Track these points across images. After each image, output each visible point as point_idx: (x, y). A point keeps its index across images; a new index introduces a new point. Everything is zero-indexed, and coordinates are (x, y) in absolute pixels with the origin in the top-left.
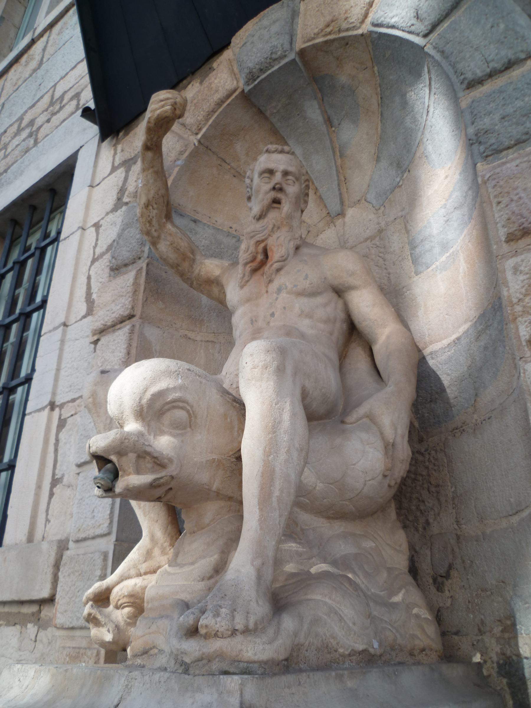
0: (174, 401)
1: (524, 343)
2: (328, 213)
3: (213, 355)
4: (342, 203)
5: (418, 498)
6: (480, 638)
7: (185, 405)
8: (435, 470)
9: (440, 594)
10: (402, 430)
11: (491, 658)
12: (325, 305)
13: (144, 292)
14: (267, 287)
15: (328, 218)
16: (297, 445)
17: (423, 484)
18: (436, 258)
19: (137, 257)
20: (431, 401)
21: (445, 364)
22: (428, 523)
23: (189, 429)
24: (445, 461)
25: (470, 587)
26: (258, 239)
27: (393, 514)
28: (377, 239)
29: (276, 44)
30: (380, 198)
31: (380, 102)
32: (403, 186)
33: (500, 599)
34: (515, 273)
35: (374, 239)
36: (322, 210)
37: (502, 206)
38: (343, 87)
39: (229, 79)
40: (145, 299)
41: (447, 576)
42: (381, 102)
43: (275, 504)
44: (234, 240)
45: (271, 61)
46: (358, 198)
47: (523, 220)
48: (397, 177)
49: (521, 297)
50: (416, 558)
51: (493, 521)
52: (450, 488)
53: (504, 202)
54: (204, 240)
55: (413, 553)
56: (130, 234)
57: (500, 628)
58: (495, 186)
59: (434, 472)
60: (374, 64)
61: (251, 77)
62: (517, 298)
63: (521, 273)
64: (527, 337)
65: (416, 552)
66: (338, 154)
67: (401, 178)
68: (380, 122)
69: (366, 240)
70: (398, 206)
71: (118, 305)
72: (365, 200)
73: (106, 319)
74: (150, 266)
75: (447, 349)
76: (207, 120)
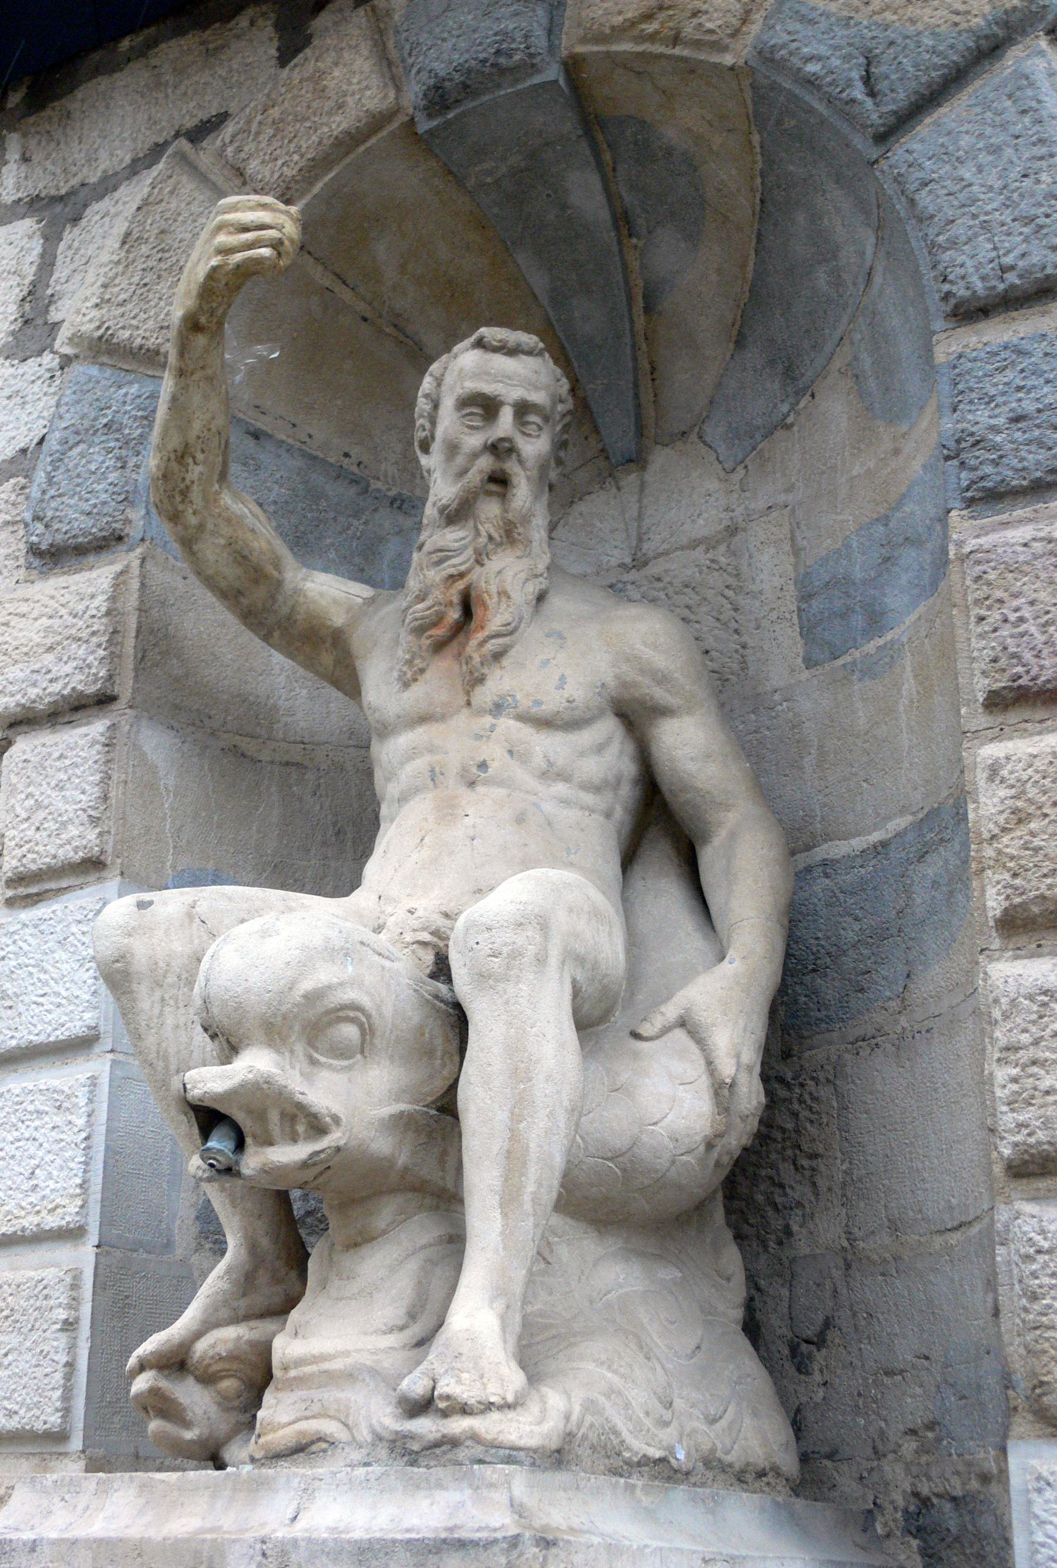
0: (344, 1007)
1: (992, 923)
2: (602, 450)
3: (301, 799)
4: (640, 431)
5: (771, 1178)
6: (876, 1463)
7: (359, 1014)
8: (812, 1122)
9: (802, 1377)
10: (751, 1056)
11: (892, 1502)
12: (600, 749)
13: (137, 637)
14: (468, 693)
15: (602, 463)
16: (566, 1103)
17: (784, 1148)
18: (855, 640)
19: (112, 534)
20: (814, 971)
21: (851, 893)
22: (788, 1232)
23: (359, 1056)
24: (835, 1104)
25: (863, 1365)
26: (453, 571)
27: (719, 1214)
28: (722, 548)
29: (511, 27)
30: (737, 442)
31: (758, 208)
32: (795, 428)
33: (918, 1390)
34: (991, 779)
35: (714, 548)
36: (586, 438)
37: (987, 629)
38: (669, 152)
39: (375, 81)
40: (140, 656)
41: (820, 1341)
42: (762, 211)
43: (528, 1206)
44: (353, 490)
45: (494, 70)
46: (684, 428)
47: (1019, 669)
48: (782, 401)
49: (996, 831)
50: (757, 1304)
51: (917, 1237)
52: (838, 1162)
53: (990, 620)
54: (276, 487)
55: (753, 1292)
56: (88, 462)
57: (914, 1445)
58: (978, 578)
59: (808, 1125)
60: (753, 127)
61: (437, 99)
62: (990, 831)
63: (1001, 782)
64: (998, 913)
65: (758, 1289)
66: (640, 303)
67: (793, 407)
68: (752, 252)
69: (694, 544)
70: (778, 475)
71: (66, 663)
72: (700, 437)
73: (33, 693)
74: (149, 566)
75: (859, 861)
76: (311, 182)
